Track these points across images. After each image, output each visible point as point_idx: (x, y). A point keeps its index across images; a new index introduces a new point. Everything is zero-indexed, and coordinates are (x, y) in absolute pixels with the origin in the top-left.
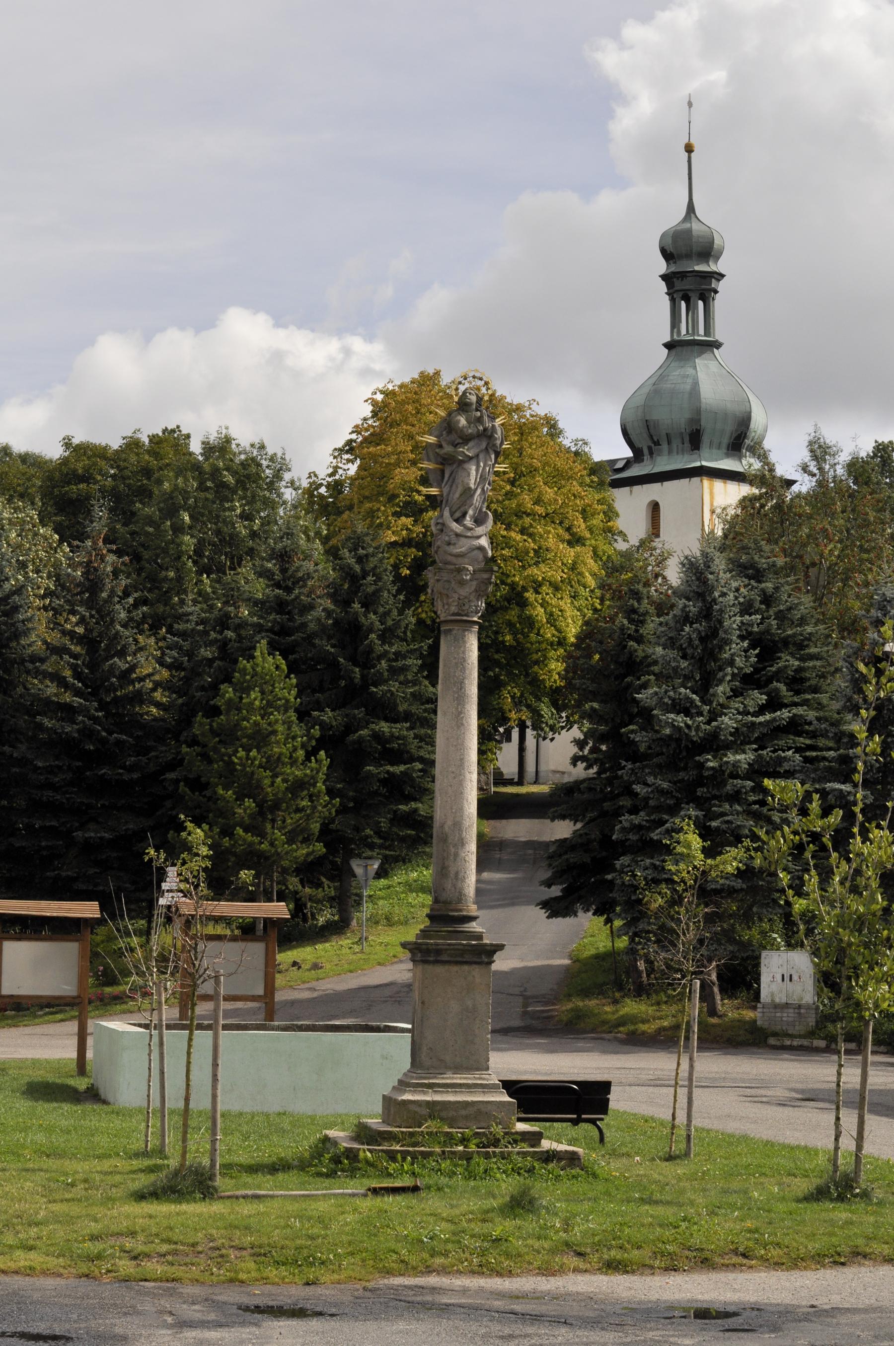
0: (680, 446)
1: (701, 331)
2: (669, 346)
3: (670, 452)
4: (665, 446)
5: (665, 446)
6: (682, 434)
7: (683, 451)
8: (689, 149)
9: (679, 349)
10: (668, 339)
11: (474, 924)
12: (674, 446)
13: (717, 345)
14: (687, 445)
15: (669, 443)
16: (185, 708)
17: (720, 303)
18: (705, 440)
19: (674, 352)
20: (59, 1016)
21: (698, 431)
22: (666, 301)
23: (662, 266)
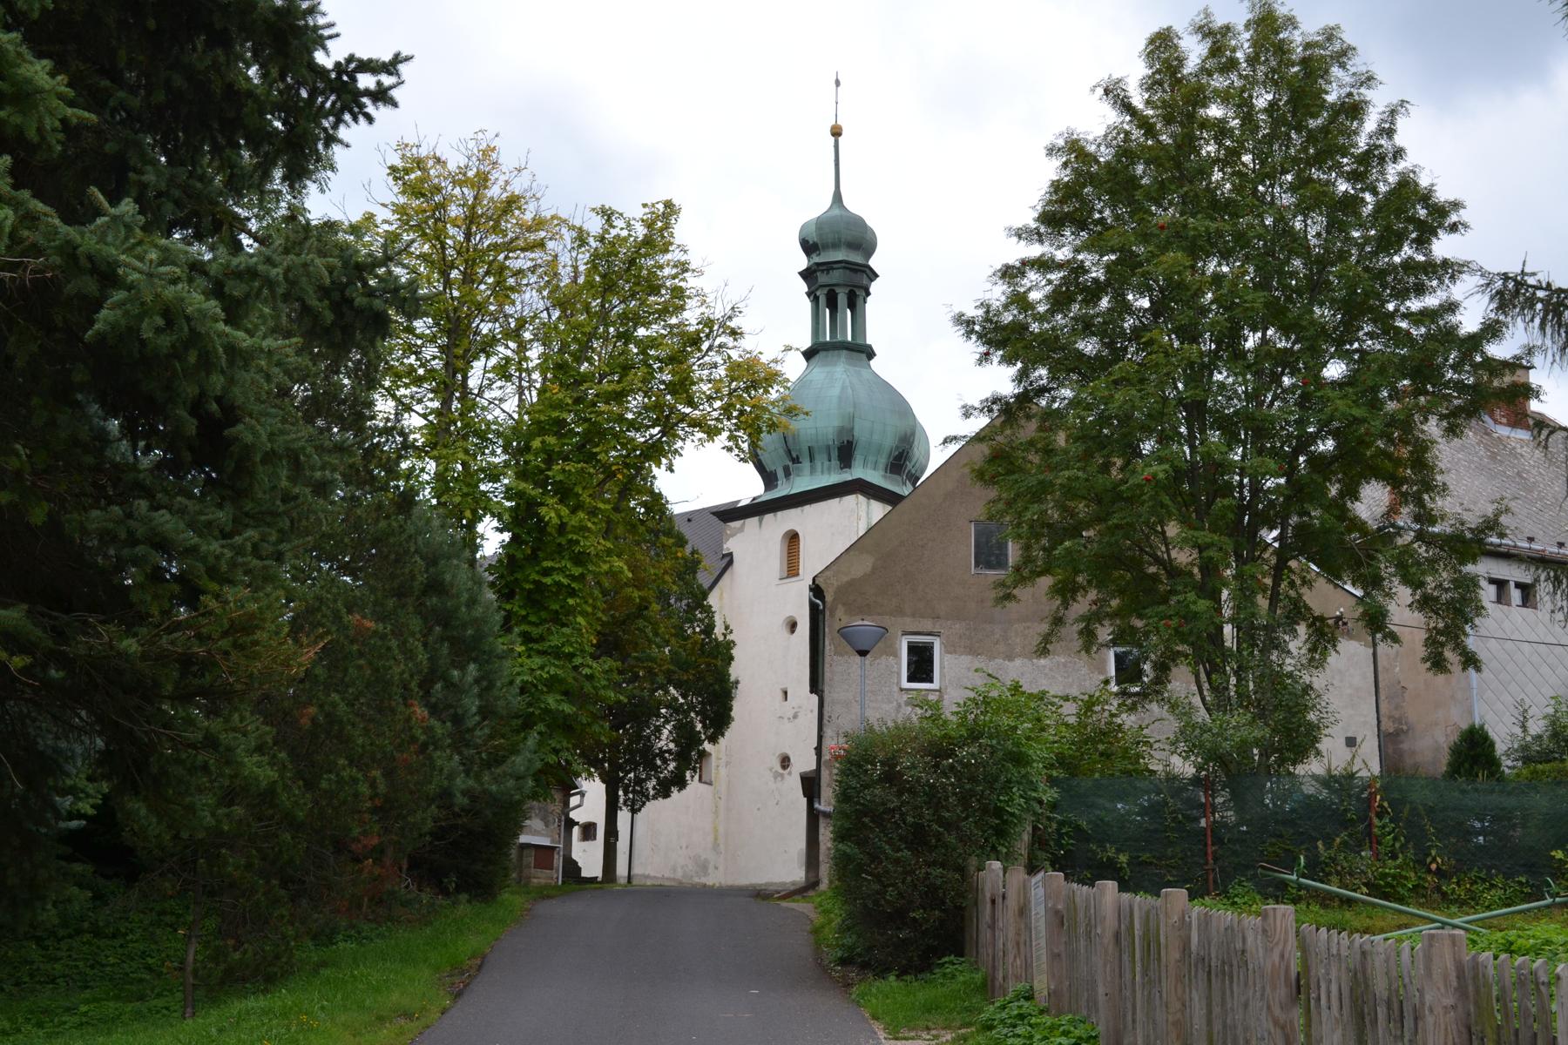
3: (813, 471)
4: (806, 464)
5: (806, 464)
6: (828, 447)
7: (829, 470)
8: (836, 132)
9: (822, 354)
14: (835, 463)
21: (850, 443)
22: (807, 304)
23: (802, 262)
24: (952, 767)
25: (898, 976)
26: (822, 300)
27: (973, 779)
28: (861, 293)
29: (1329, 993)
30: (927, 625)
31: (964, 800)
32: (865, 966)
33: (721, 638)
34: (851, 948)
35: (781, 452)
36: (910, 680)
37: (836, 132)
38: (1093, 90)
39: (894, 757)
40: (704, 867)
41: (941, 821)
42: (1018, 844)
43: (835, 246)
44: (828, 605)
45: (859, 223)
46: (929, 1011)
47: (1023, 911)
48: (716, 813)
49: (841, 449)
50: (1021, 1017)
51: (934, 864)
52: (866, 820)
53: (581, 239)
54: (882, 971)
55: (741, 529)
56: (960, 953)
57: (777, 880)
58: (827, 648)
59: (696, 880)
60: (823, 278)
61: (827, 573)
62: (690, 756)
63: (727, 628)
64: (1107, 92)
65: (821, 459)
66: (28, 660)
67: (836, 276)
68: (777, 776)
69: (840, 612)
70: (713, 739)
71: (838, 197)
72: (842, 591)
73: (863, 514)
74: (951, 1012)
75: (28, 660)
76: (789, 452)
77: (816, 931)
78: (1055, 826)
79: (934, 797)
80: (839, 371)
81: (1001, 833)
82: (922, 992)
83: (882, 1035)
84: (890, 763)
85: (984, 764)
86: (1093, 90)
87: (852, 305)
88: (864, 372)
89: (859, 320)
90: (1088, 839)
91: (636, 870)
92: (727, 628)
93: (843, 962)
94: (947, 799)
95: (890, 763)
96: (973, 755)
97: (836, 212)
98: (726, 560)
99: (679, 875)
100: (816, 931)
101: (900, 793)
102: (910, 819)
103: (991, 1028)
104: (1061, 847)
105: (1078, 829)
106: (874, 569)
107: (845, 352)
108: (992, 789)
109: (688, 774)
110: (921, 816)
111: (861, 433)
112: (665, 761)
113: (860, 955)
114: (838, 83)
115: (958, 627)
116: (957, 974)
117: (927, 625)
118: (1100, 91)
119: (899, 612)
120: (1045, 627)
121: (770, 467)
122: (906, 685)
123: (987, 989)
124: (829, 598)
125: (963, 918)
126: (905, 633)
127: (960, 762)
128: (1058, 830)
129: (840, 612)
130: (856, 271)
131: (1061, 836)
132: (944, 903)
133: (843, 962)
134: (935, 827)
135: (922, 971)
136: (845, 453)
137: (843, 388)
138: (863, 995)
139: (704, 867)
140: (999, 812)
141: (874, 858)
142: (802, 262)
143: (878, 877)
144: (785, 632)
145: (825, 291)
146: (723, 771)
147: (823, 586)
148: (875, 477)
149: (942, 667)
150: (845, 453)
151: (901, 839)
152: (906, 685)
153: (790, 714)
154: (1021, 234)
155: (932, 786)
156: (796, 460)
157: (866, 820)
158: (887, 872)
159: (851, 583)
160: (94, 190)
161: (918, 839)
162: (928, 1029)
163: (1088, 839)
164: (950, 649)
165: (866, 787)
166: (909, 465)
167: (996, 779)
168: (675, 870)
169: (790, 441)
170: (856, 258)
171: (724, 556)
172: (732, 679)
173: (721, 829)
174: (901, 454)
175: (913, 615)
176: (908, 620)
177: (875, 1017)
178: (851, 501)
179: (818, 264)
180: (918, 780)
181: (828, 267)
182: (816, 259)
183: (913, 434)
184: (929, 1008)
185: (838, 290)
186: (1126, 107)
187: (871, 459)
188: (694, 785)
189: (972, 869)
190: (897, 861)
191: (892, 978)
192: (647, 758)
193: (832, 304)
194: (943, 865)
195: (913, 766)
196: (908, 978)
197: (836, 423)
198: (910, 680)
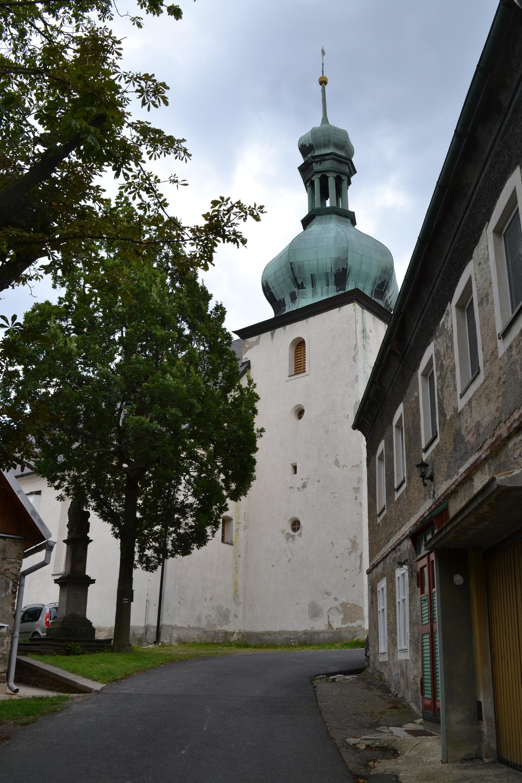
5: (309, 289)
6: (327, 274)
8: (323, 82)
9: (317, 218)
15: (313, 285)
21: (345, 271)
35: (289, 281)
37: (323, 82)
40: (225, 616)
43: (326, 145)
48: (236, 569)
49: (336, 275)
53: (144, 162)
55: (257, 342)
57: (290, 629)
59: (219, 628)
60: (317, 167)
62: (210, 512)
66: (385, 580)
67: (327, 165)
68: (288, 537)
70: (235, 496)
71: (325, 120)
73: (359, 319)
75: (385, 580)
76: (295, 280)
80: (329, 229)
87: (339, 182)
91: (165, 621)
99: (204, 624)
109: (209, 530)
111: (353, 262)
112: (184, 515)
114: (323, 53)
121: (279, 297)
136: (341, 276)
139: (225, 616)
142: (301, 161)
144: (294, 418)
145: (319, 175)
146: (242, 533)
153: (300, 485)
156: (301, 286)
160: (121, 425)
168: (199, 620)
169: (296, 270)
172: (257, 426)
173: (240, 583)
185: (328, 175)
188: (214, 542)
192: (170, 512)
197: (333, 255)
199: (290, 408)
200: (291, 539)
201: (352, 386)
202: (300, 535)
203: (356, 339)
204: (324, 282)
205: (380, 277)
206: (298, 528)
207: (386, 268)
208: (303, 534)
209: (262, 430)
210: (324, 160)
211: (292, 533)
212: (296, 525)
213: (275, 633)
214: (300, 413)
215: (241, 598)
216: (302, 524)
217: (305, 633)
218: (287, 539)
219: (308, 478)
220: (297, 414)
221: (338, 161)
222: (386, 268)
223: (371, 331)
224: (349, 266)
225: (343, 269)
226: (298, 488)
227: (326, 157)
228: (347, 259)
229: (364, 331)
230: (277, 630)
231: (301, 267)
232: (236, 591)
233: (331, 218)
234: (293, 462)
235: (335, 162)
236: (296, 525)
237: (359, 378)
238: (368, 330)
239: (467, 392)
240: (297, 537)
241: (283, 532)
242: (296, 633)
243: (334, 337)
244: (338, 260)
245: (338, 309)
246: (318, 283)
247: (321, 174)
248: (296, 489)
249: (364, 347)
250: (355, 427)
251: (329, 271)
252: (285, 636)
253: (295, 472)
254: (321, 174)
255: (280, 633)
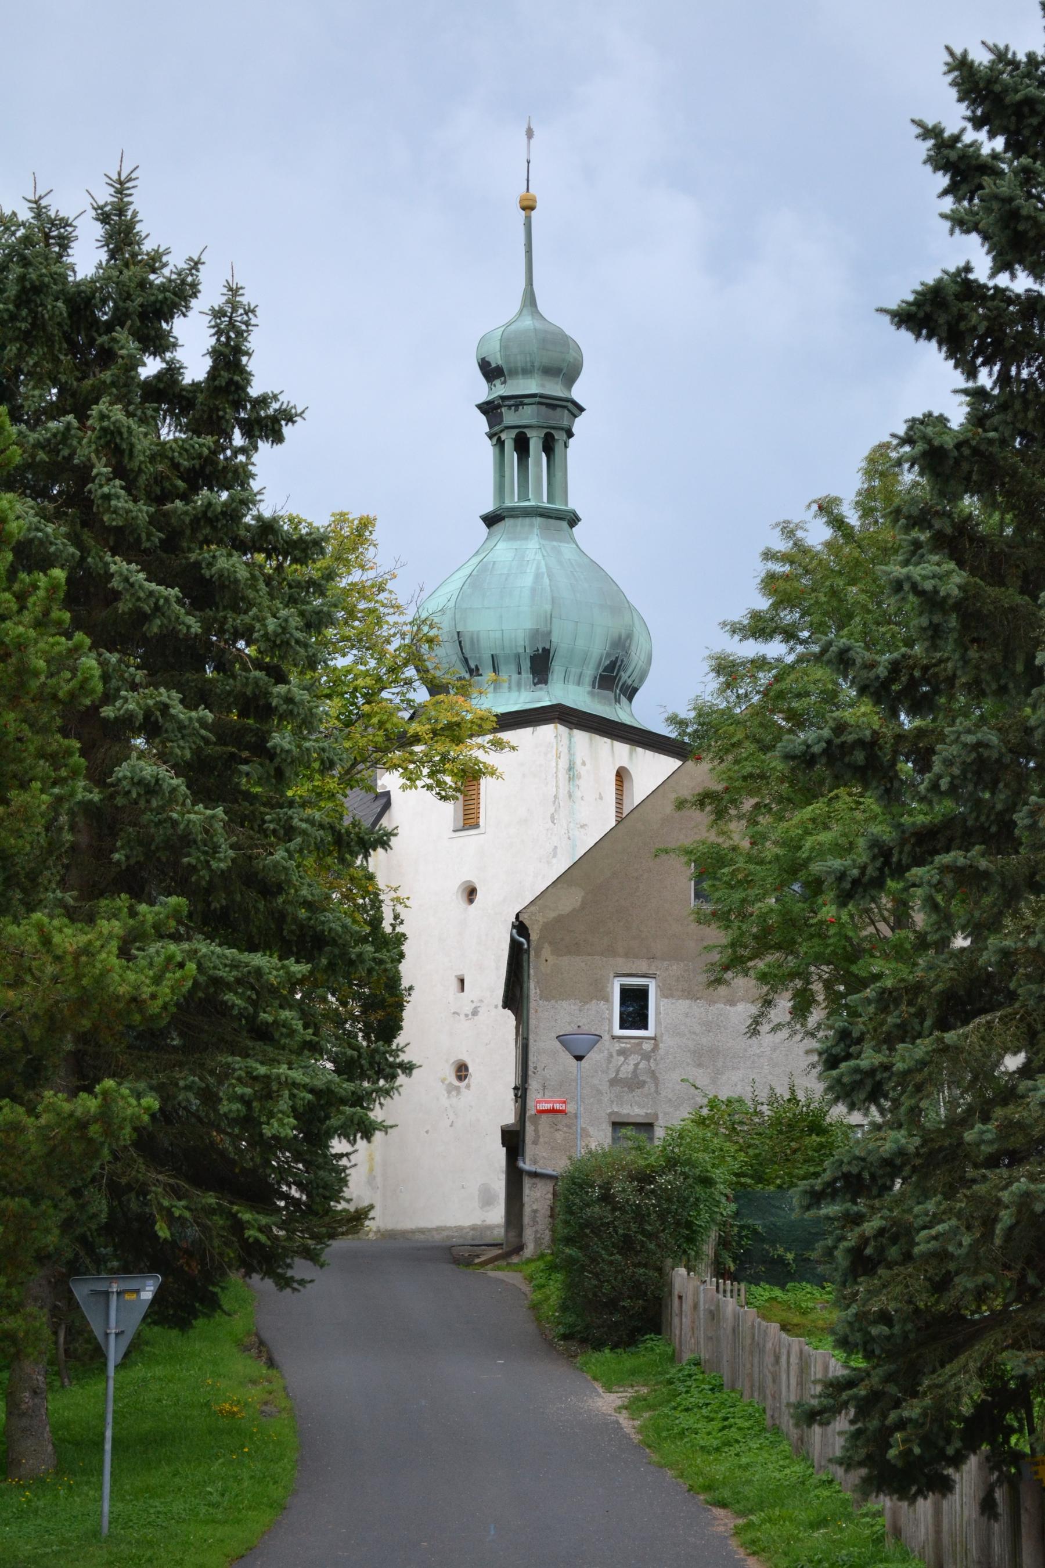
0: (515, 676)
1: (545, 499)
2: (491, 520)
3: (496, 684)
4: (488, 675)
5: (488, 675)
6: (518, 656)
7: (519, 685)
8: (528, 207)
9: (508, 522)
10: (489, 506)
11: (619, 1403)
12: (504, 676)
13: (573, 520)
14: (527, 676)
15: (495, 669)
16: (42, 456)
17: (577, 452)
18: (557, 670)
19: (497, 527)
20: (525, 964)
21: (546, 652)
22: (488, 447)
23: (483, 391)
24: (653, 1191)
25: (611, 1349)
26: (509, 445)
27: (669, 1200)
28: (559, 436)
29: (788, 1362)
30: (643, 966)
31: (662, 1216)
32: (584, 1341)
33: (388, 929)
34: (571, 1326)
36: (622, 1027)
37: (528, 207)
38: (809, 506)
39: (608, 1183)
41: (643, 1232)
42: (705, 1248)
43: (526, 372)
44: (533, 944)
45: (562, 341)
46: (633, 1374)
47: (696, 1306)
50: (690, 1376)
51: (639, 1265)
52: (588, 1231)
54: (598, 1346)
56: (658, 1332)
58: (532, 992)
60: (510, 417)
61: (532, 908)
63: (396, 917)
64: (820, 508)
65: (507, 672)
67: (527, 415)
68: (451, 1089)
69: (546, 952)
71: (530, 300)
72: (548, 928)
74: (649, 1374)
77: (535, 1307)
78: (736, 1229)
79: (640, 1215)
80: (525, 552)
81: (691, 1240)
82: (628, 1360)
83: (601, 1390)
84: (606, 1186)
85: (678, 1189)
86: (809, 506)
87: (549, 447)
88: (567, 550)
89: (559, 474)
90: (763, 1240)
92: (396, 917)
93: (565, 1337)
94: (649, 1215)
95: (606, 1186)
96: (669, 1182)
97: (528, 322)
98: (384, 801)
100: (535, 1307)
101: (614, 1210)
102: (621, 1231)
103: (672, 1383)
104: (742, 1247)
105: (755, 1232)
106: (583, 906)
107: (539, 520)
108: (683, 1207)
110: (629, 1229)
111: (561, 639)
113: (580, 1332)
115: (676, 969)
116: (653, 1346)
117: (643, 966)
118: (815, 507)
119: (610, 952)
120: (754, 1010)
122: (618, 1032)
123: (673, 1358)
124: (534, 936)
125: (660, 1305)
126: (618, 975)
127: (660, 1187)
128: (739, 1232)
129: (546, 952)
130: (554, 407)
131: (741, 1238)
132: (645, 1294)
133: (565, 1337)
134: (640, 1237)
135: (629, 1345)
137: (538, 577)
138: (585, 1364)
140: (689, 1225)
141: (593, 1260)
142: (483, 391)
143: (596, 1275)
144: (461, 902)
145: (513, 433)
147: (527, 923)
148: (578, 696)
149: (658, 1013)
150: (540, 664)
151: (614, 1245)
152: (618, 1032)
153: (468, 1009)
154: (735, 629)
155: (638, 1206)
156: (474, 672)
157: (588, 1231)
158: (603, 1271)
159: (559, 920)
161: (627, 1245)
162: (632, 1386)
163: (763, 1240)
164: (666, 992)
165: (588, 1205)
166: (624, 676)
167: (687, 1200)
170: (554, 389)
171: (378, 796)
172: (405, 984)
173: (378, 1158)
174: (613, 664)
175: (626, 955)
176: (620, 961)
177: (595, 1379)
178: (548, 732)
179: (503, 398)
180: (628, 1200)
181: (517, 401)
182: (502, 389)
183: (630, 636)
184: (633, 1372)
185: (530, 433)
186: (838, 523)
187: (574, 671)
189: (668, 1269)
190: (611, 1263)
191: (607, 1351)
193: (522, 446)
194: (645, 1266)
195: (624, 1190)
196: (619, 1351)
198: (622, 1027)
199: (454, 886)
200: (454, 1093)
201: (548, 863)
202: (468, 1087)
203: (557, 786)
204: (513, 667)
205: (608, 655)
206: (466, 1076)
207: (620, 637)
208: (472, 1085)
209: (411, 988)
210: (523, 404)
211: (456, 1083)
212: (462, 1071)
213: (430, 1230)
214: (471, 893)
215: (379, 1180)
216: (471, 1070)
217: (474, 1228)
218: (449, 1092)
219: (481, 1001)
220: (465, 895)
221: (548, 405)
222: (620, 637)
223: (584, 764)
224: (554, 644)
225: (544, 649)
226: (466, 1015)
227: (526, 401)
228: (550, 633)
229: (571, 768)
230: (434, 1226)
231: (475, 642)
232: (371, 1170)
233: (532, 525)
234: (459, 973)
235: (544, 408)
236: (462, 1071)
237: (559, 850)
238: (578, 762)
239: (532, 1059)
240: (463, 1090)
241: (443, 1081)
242: (460, 1228)
243: (524, 776)
244: (535, 634)
245: (530, 729)
246: (503, 668)
247: (517, 431)
248: (462, 1017)
249: (570, 796)
250: (504, 1007)
251: (521, 650)
252: (445, 1233)
253: (463, 990)
254: (517, 431)
255: (438, 1229)
